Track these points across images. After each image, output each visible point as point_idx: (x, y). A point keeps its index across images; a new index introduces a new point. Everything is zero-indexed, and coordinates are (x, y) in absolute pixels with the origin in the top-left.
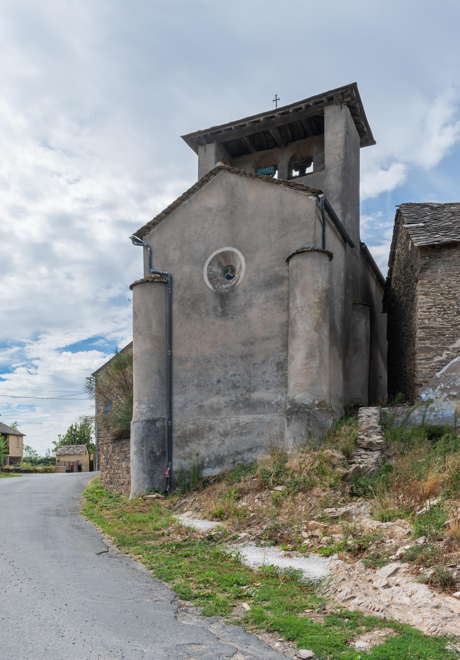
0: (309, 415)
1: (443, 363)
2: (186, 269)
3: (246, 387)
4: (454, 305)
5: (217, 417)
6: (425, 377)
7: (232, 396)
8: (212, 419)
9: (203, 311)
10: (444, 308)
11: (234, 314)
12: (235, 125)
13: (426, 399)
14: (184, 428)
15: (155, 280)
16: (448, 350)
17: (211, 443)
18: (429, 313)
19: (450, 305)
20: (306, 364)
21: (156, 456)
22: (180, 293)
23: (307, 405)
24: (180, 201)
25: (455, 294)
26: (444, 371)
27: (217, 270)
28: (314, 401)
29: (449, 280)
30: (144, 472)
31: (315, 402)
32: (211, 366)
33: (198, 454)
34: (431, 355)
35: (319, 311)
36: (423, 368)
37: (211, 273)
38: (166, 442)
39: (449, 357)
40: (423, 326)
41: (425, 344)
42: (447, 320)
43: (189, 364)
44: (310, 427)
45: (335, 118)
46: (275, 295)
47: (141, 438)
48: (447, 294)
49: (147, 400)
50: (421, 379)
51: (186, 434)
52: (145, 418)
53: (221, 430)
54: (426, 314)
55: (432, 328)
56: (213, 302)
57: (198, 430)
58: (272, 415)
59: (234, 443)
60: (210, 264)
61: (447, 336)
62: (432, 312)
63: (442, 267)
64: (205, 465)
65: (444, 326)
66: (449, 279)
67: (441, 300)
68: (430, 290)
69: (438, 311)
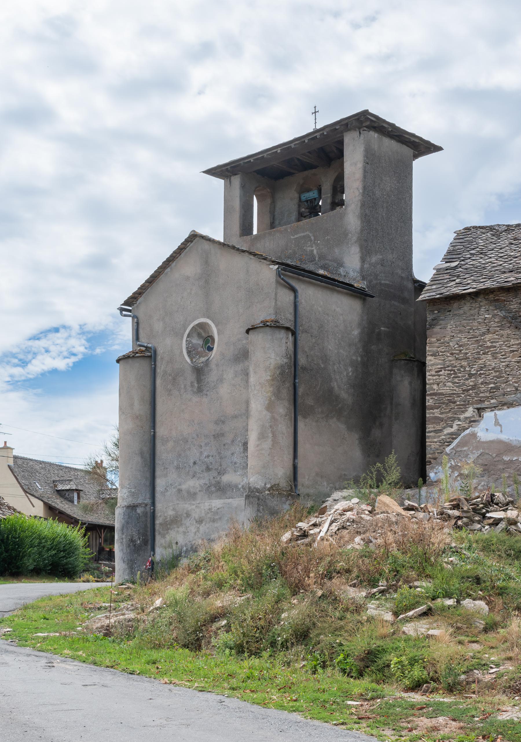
0: (259, 499)
1: (454, 436)
2: (168, 341)
3: (218, 469)
4: (465, 367)
5: (193, 502)
6: (434, 453)
7: (206, 479)
8: (189, 504)
9: (182, 387)
10: (455, 370)
11: (208, 391)
12: (254, 158)
13: (435, 480)
14: (166, 515)
15: (137, 355)
16: (459, 420)
17: (189, 530)
18: (437, 377)
19: (462, 367)
20: (258, 446)
21: (135, 544)
22: (163, 367)
23: (258, 489)
24: (161, 270)
25: (467, 353)
26: (454, 445)
27: (197, 341)
28: (265, 484)
29: (460, 337)
30: (124, 562)
31: (267, 486)
32: (189, 446)
33: (177, 543)
34: (440, 426)
35: (271, 389)
36: (432, 442)
37: (191, 345)
38: (149, 530)
39: (460, 429)
40: (432, 392)
41: (433, 413)
42: (457, 385)
43: (170, 444)
44: (260, 512)
45: (354, 145)
46: (242, 370)
47: (121, 525)
48: (458, 354)
49: (129, 484)
50: (430, 456)
51: (167, 521)
52: (126, 504)
53: (197, 517)
54: (434, 378)
55: (442, 394)
56: (190, 377)
57: (177, 517)
58: (239, 499)
59: (207, 531)
60: (188, 336)
61: (458, 403)
62: (441, 375)
63: (452, 322)
64: (183, 554)
65: (455, 392)
66: (459, 335)
67: (451, 361)
68: (439, 349)
69: (448, 374)
